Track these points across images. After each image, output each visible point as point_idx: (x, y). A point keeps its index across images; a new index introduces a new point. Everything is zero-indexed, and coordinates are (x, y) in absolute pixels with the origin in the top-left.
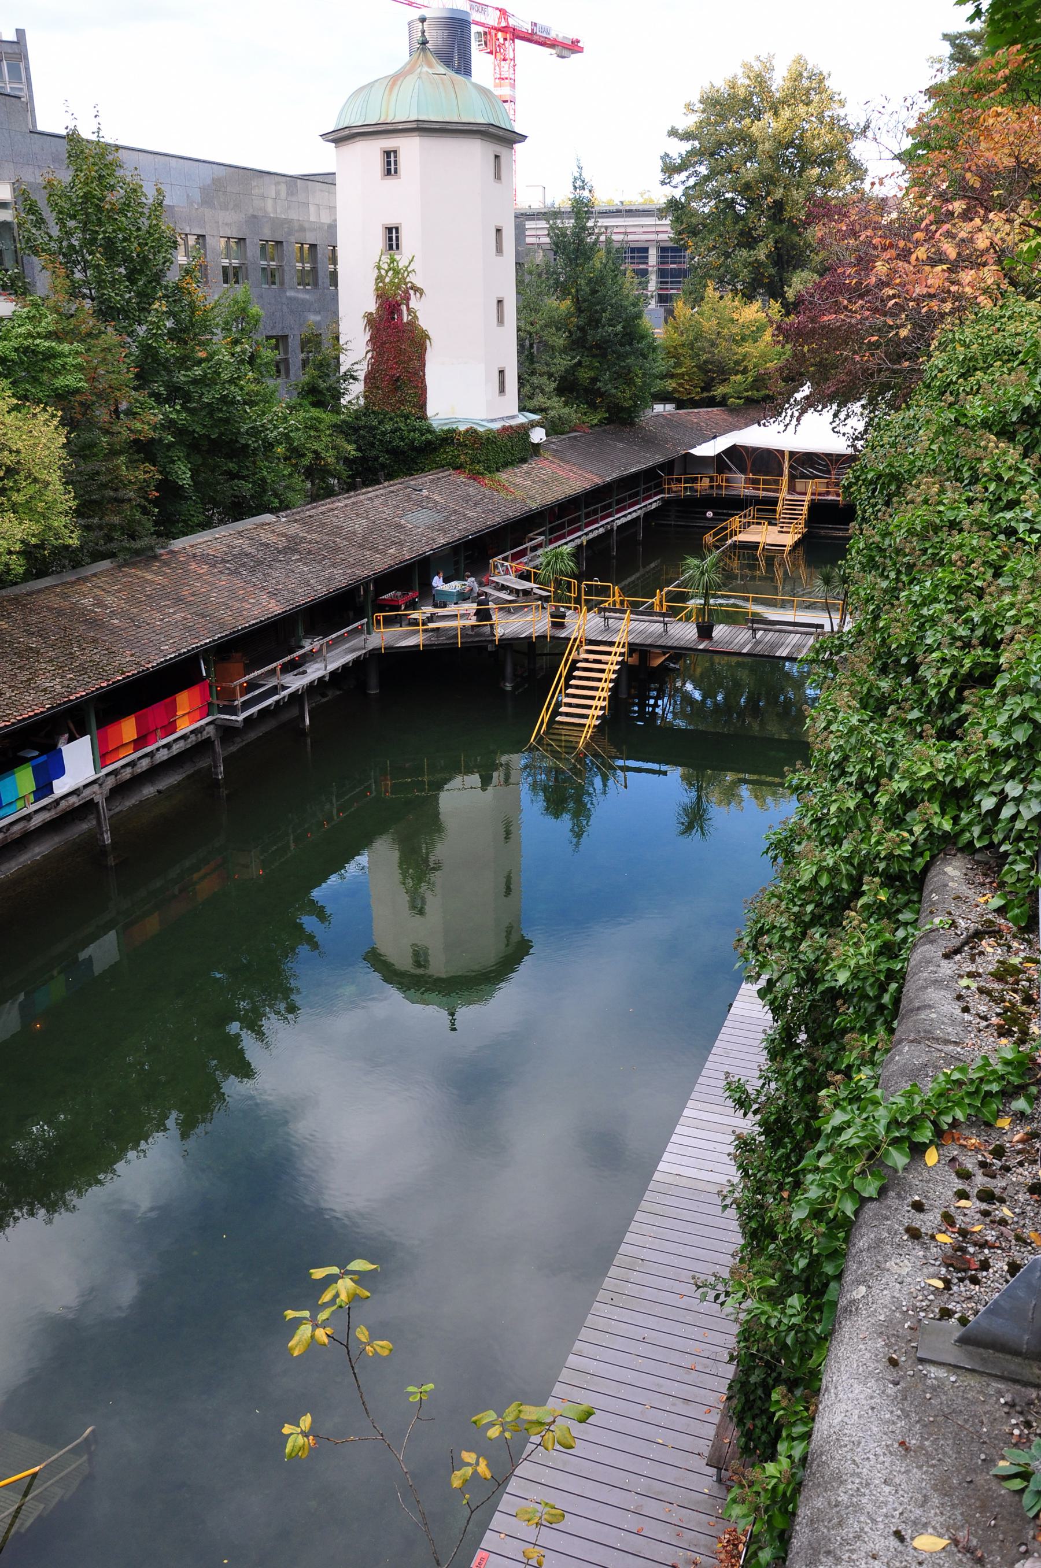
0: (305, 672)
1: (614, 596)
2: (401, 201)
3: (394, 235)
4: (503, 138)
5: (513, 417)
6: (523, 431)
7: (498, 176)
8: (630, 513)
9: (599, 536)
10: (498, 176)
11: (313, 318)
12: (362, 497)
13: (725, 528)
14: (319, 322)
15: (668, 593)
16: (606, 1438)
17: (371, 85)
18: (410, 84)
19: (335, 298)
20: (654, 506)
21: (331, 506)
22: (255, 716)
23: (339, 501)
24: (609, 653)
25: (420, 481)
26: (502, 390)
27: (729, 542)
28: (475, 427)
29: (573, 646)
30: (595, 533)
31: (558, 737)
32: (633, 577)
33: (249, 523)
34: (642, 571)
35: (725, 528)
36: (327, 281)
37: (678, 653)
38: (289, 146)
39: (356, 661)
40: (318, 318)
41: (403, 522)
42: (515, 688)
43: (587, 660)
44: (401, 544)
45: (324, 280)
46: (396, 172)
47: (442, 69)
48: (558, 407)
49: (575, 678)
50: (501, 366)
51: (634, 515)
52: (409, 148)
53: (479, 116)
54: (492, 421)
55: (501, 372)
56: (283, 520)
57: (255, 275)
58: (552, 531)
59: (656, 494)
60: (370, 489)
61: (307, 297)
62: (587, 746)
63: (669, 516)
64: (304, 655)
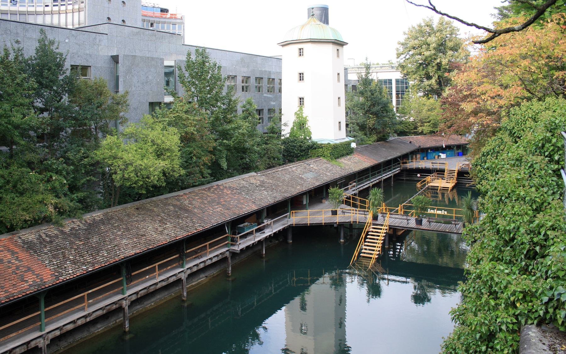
0: (264, 233)
5: (344, 139)
6: (349, 144)
7: (338, 56)
9: (377, 183)
10: (338, 56)
11: (273, 103)
13: (425, 181)
20: (397, 172)
24: (381, 229)
26: (340, 129)
27: (427, 186)
30: (375, 182)
34: (393, 198)
35: (425, 181)
37: (408, 231)
39: (284, 229)
40: (274, 103)
42: (344, 242)
43: (372, 232)
44: (302, 185)
45: (277, 90)
47: (319, 23)
48: (360, 134)
49: (368, 238)
51: (390, 175)
53: (331, 37)
57: (253, 89)
58: (358, 181)
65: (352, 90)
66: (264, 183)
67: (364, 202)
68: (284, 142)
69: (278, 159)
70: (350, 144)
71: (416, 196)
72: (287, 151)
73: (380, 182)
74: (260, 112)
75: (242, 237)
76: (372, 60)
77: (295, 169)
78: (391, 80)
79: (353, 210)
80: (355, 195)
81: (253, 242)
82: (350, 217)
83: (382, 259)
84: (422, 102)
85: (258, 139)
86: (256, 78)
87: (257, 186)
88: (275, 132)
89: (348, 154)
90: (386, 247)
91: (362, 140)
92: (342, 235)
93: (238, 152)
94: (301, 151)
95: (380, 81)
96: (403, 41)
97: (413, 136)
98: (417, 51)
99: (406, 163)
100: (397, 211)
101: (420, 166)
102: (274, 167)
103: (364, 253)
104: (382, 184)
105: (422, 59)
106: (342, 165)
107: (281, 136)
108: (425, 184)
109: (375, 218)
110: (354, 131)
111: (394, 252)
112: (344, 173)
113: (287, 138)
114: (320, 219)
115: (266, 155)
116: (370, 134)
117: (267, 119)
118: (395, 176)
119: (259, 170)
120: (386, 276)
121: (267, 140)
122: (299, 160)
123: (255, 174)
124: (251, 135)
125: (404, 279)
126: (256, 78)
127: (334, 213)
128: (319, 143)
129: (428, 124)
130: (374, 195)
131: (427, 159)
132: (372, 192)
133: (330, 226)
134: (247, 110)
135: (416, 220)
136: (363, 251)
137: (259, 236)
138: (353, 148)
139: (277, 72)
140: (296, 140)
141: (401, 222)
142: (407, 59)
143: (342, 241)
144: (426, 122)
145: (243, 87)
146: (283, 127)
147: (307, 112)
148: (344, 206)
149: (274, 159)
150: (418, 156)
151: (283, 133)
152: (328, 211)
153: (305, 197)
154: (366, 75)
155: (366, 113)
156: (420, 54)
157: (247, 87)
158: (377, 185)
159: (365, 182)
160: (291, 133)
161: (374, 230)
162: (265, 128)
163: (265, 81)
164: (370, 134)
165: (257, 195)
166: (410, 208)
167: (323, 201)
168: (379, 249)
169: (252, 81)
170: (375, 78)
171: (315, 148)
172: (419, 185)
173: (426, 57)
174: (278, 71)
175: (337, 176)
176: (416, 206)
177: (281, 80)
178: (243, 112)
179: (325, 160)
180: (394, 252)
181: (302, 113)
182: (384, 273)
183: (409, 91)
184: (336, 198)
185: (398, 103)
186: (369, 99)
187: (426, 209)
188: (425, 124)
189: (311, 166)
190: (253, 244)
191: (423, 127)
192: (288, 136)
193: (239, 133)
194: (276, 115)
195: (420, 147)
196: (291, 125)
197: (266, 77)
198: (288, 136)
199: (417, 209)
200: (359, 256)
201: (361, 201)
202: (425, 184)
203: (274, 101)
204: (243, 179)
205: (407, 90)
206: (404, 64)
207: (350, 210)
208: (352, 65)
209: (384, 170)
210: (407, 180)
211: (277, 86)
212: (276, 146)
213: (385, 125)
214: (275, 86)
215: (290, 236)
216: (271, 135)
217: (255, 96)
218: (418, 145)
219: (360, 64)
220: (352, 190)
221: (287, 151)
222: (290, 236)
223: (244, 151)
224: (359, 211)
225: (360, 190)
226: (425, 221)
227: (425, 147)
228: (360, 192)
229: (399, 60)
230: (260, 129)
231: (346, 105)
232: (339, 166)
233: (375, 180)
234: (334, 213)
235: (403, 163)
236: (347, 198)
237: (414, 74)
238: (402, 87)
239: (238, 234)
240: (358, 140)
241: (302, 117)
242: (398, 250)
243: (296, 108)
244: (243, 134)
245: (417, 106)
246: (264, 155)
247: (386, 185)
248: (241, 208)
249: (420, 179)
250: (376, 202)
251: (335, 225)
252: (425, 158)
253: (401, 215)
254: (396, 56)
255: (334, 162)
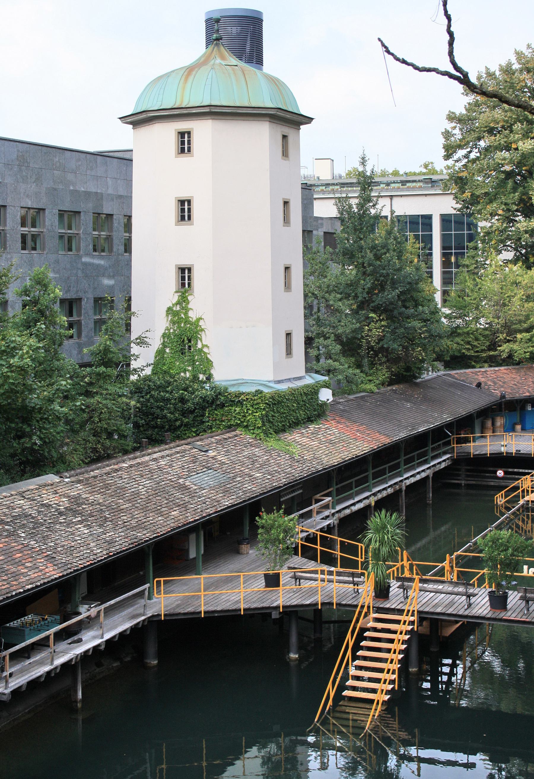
0: (80, 641)
1: (402, 560)
2: (192, 176)
3: (186, 207)
4: (289, 120)
5: (300, 378)
6: (313, 392)
7: (285, 153)
8: (419, 473)
9: (388, 496)
10: (285, 153)
11: (107, 282)
12: (147, 458)
13: (516, 488)
14: (113, 287)
15: (458, 557)
16: (483, 602)
17: (168, 75)
18: (203, 73)
19: (128, 264)
20: (443, 465)
21: (116, 467)
22: (24, 689)
23: (124, 461)
24: (398, 622)
25: (207, 441)
26: (289, 352)
27: (521, 502)
28: (261, 388)
29: (360, 613)
30: (384, 494)
31: (345, 716)
32: (424, 542)
33: (32, 484)
34: (432, 535)
35: (516, 488)
36: (122, 248)
37: (470, 626)
38: (98, 132)
39: (134, 629)
40: (111, 282)
41: (187, 483)
42: (300, 660)
43: (375, 630)
44: (184, 506)
45: (118, 247)
46: (189, 150)
47: (234, 61)
48: (345, 366)
49: (362, 648)
50: (288, 329)
51: (423, 475)
52: (202, 131)
53: (266, 100)
54: (279, 382)
55: (288, 335)
56: (67, 480)
57: (52, 242)
58: (339, 492)
59: (445, 453)
60: (156, 449)
61: (102, 262)
62: (375, 729)
63: (459, 475)
64: (80, 622)
65: (324, 245)
66: (79, 505)
67: (354, 550)
68: (138, 390)
69: (122, 436)
70: (316, 393)
71: (491, 531)
72: (146, 414)
73: (397, 494)
74: (70, 305)
75: (16, 657)
76: (380, 164)
77: (166, 461)
78: (429, 217)
79: (323, 572)
80: (329, 529)
81: (47, 668)
82: (313, 592)
83: (401, 702)
84: (512, 278)
85: (64, 383)
86: (62, 214)
87: (61, 514)
88: (114, 362)
89: (310, 420)
90: (413, 670)
91: (349, 381)
92: (294, 639)
93: (8, 419)
94: (184, 413)
95: (401, 220)
96: (460, 110)
97: (486, 368)
98: (500, 139)
99: (467, 440)
100: (441, 572)
101: (503, 449)
102: (109, 457)
103: (354, 689)
104: (403, 500)
105: (511, 162)
106: (296, 450)
107: (128, 374)
108: (517, 496)
109: (382, 592)
110: (329, 356)
111: (435, 683)
112: (299, 472)
113: (147, 379)
114: (234, 598)
115: (88, 427)
116: (372, 364)
117: (92, 325)
118: (438, 475)
119: (69, 467)
120: (413, 751)
121: (91, 384)
122: (179, 438)
123: (56, 479)
124: (46, 371)
125: (461, 757)
126: (62, 214)
127: (272, 581)
128: (232, 390)
129: (527, 335)
130: (377, 531)
131: (523, 429)
132: (375, 520)
133: (259, 617)
134: (35, 302)
135: (491, 594)
136: (350, 683)
137: (65, 652)
138: (325, 404)
139: (120, 197)
140: (169, 383)
141: (452, 603)
142: (474, 161)
143: (294, 656)
144: (521, 332)
145: (24, 237)
146: (135, 349)
147: (199, 306)
148: (297, 561)
149: (110, 435)
150: (500, 422)
151: (134, 364)
152: (255, 576)
153: (193, 537)
154: (361, 206)
155: (361, 306)
156: (508, 148)
157: (34, 237)
158: (387, 503)
159: (358, 493)
160: (156, 365)
161: (380, 625)
162: (85, 351)
163: (87, 220)
164: (372, 364)
165: (60, 537)
166: (476, 563)
167: (244, 548)
168: (394, 677)
169: (50, 222)
170: (386, 212)
171: (222, 406)
172: (500, 499)
173: (524, 156)
174: (122, 192)
175: (282, 480)
176: (490, 559)
177: (130, 217)
178: (24, 306)
179: (248, 437)
180: (435, 683)
181: (186, 310)
182: (407, 743)
183: (476, 248)
184: (276, 541)
185: (447, 280)
186: (369, 269)
187: (517, 567)
188: (519, 336)
189: (211, 453)
190: (48, 673)
191: (511, 345)
192: (148, 371)
193: (10, 366)
194: (116, 315)
195: (503, 396)
196: (156, 343)
197: (87, 208)
198: (148, 371)
199: (494, 567)
200: (338, 697)
201: (344, 548)
202: (517, 496)
203: (109, 277)
204: (22, 495)
205: (471, 244)
206: (464, 174)
207: (316, 572)
208: (326, 176)
209: (407, 462)
210: (469, 486)
211: (118, 235)
212: (115, 401)
213: (411, 340)
214: (114, 234)
215: (152, 648)
216: (102, 369)
217: (57, 262)
218: (498, 393)
219: (349, 174)
220: (321, 517)
221: (146, 414)
222: (152, 648)
223: (27, 414)
224: (339, 574)
225: (342, 515)
226: (514, 598)
227: (517, 396)
228: (342, 521)
229: (450, 162)
230: (70, 356)
231: (306, 285)
232: (287, 452)
233: (383, 489)
234: (272, 581)
235: (460, 441)
236: (308, 539)
237: (491, 201)
238: (459, 237)
239: (6, 649)
240: (339, 381)
241: (187, 321)
242: (445, 678)
243: (170, 297)
244: (22, 370)
245: (496, 287)
246: (82, 425)
247: (412, 505)
248: (16, 575)
249: (503, 484)
250: (385, 550)
251: (275, 615)
252: (518, 427)
253: (451, 582)
254: (443, 152)
255: (272, 443)
